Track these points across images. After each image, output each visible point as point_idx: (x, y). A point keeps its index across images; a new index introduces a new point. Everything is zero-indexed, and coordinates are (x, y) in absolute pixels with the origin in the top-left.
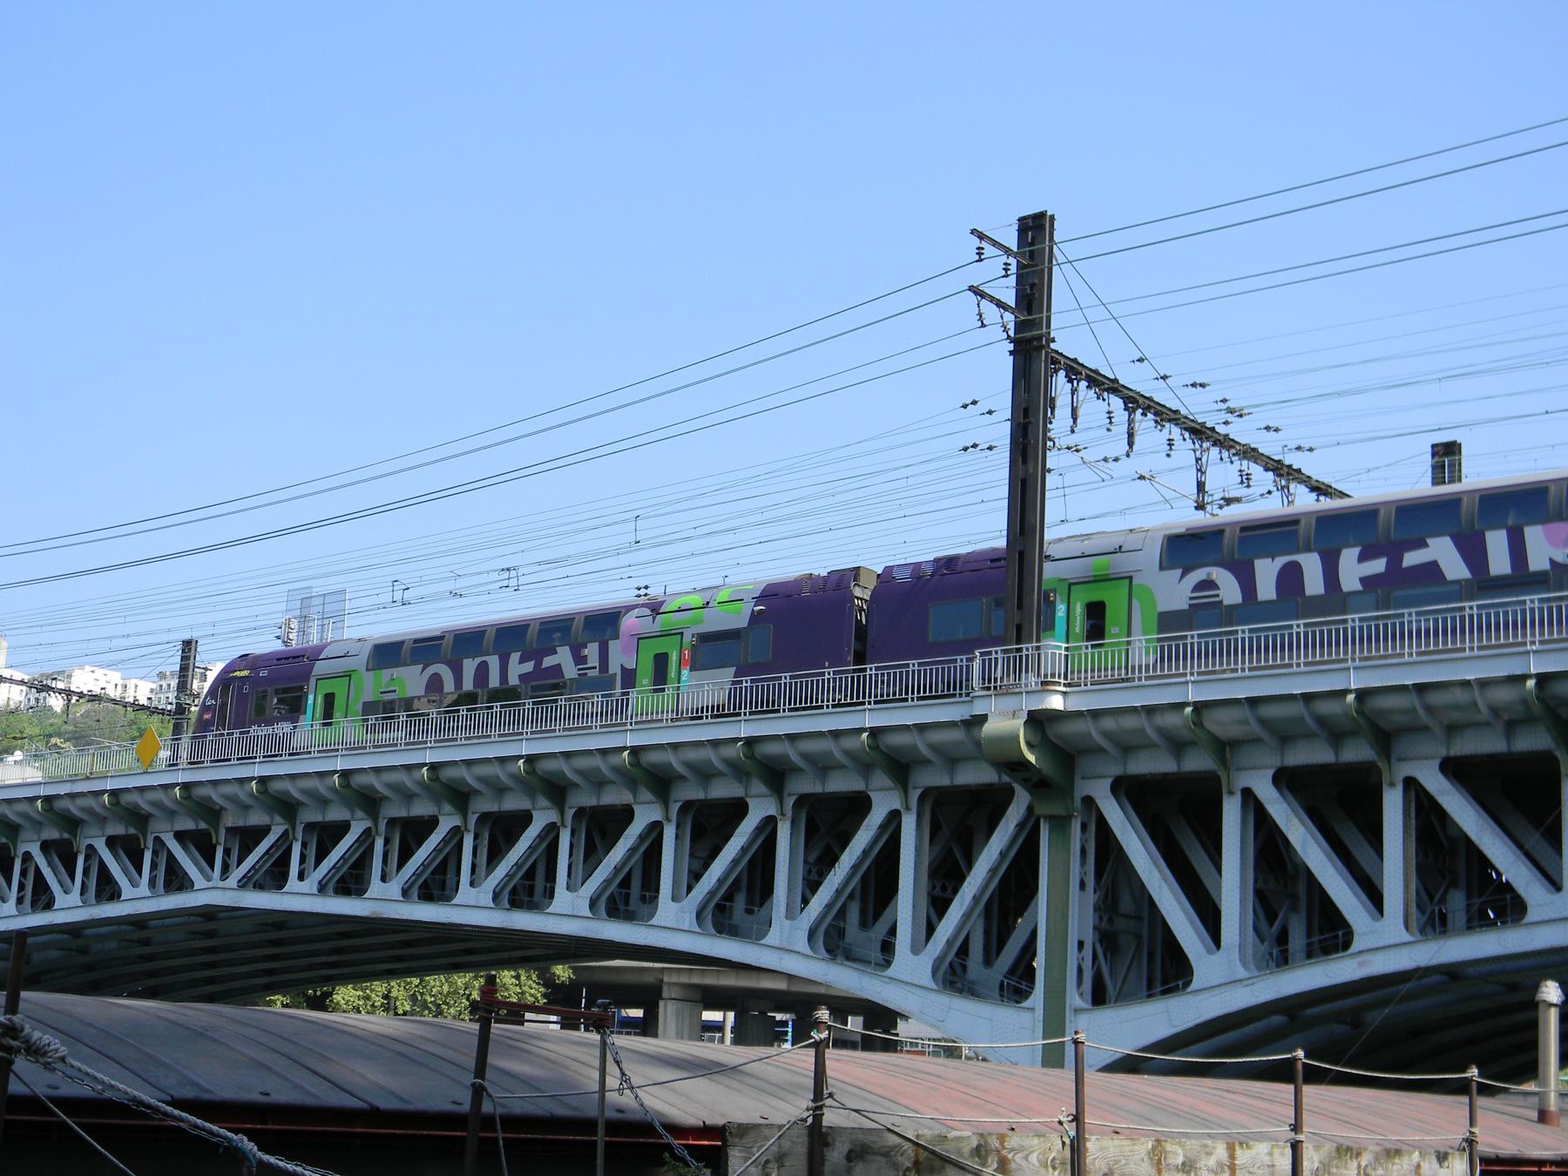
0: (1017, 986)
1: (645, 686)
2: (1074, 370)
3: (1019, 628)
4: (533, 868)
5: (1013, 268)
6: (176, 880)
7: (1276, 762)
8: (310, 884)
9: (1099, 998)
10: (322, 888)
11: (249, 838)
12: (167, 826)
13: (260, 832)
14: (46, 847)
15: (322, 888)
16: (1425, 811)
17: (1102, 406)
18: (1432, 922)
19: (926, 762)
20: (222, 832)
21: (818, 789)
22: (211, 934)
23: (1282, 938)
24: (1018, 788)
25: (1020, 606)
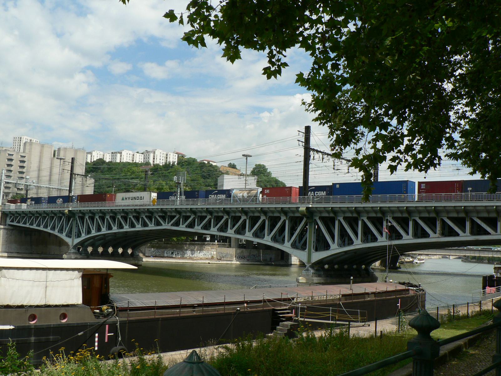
0: (71, 237)
1: (412, 290)
2: (314, 150)
3: (305, 193)
5: (304, 136)
6: (158, 224)
7: (343, 215)
8: (184, 226)
9: (317, 250)
11: (172, 217)
12: (157, 214)
13: (174, 217)
14: (122, 217)
15: (186, 226)
16: (365, 226)
17: (318, 155)
18: (365, 240)
20: (167, 216)
21: (272, 215)
22: (138, 233)
23: (344, 241)
25: (305, 190)
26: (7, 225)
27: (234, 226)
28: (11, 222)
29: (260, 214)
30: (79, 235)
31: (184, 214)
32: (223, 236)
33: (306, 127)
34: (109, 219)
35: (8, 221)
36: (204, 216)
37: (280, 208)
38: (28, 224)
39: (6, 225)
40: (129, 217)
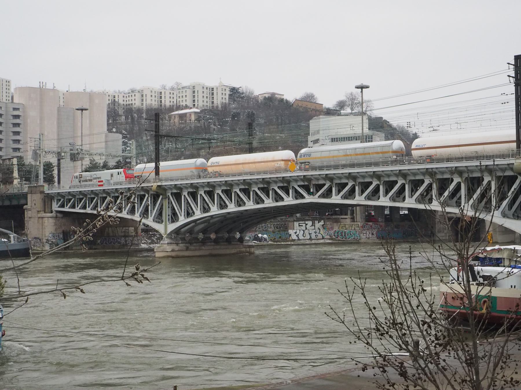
4: (238, 201)
10: (80, 209)
12: (296, 184)
19: (409, 175)
20: (312, 185)
21: (388, 180)
24: (519, 176)
26: (54, 212)
27: (249, 198)
28: (59, 207)
29: (398, 178)
30: (174, 217)
31: (361, 180)
32: (371, 206)
33: (515, 56)
34: (204, 195)
35: (55, 207)
36: (419, 180)
37: (324, 174)
38: (90, 209)
39: (52, 212)
40: (253, 189)
